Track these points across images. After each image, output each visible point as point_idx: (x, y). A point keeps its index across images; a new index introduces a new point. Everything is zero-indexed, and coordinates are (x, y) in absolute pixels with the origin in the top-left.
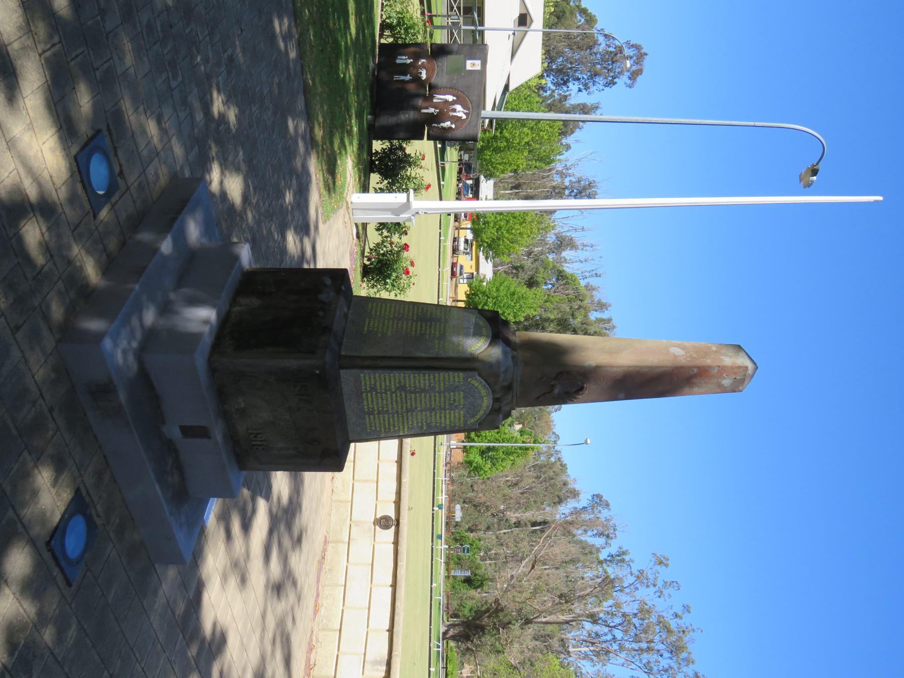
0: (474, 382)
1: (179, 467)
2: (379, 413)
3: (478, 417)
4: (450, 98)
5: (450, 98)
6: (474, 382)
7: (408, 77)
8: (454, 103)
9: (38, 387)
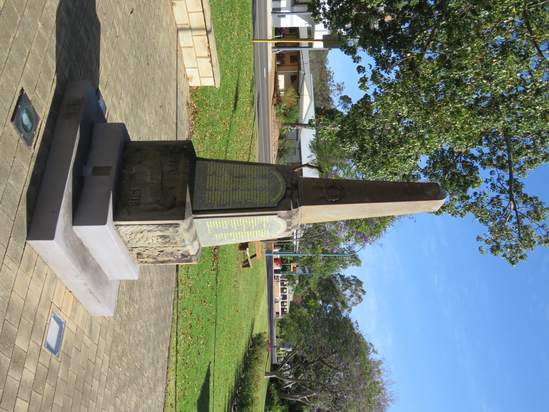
0: (274, 173)
2: (215, 190)
3: (277, 197)
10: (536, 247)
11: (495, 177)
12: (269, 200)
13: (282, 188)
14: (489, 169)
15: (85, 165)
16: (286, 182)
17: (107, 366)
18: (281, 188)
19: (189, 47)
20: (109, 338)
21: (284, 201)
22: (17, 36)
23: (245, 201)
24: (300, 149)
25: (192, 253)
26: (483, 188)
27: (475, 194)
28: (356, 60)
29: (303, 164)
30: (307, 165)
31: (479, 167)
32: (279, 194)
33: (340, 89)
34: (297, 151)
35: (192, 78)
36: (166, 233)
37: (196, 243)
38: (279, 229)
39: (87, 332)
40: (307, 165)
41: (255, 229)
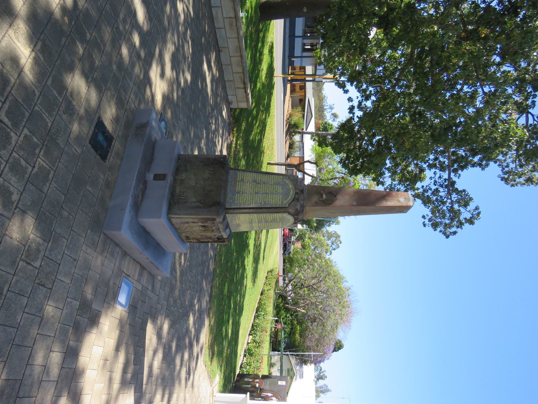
0: (286, 181)
1: (144, 191)
2: (243, 193)
3: (288, 200)
4: (270, 395)
5: (270, 395)
6: (286, 181)
7: (250, 386)
8: (271, 397)
9: (36, 44)
10: (465, 224)
11: (438, 176)
12: (282, 202)
13: (292, 193)
14: (433, 170)
15: (148, 172)
16: (295, 188)
17: (165, 309)
18: (291, 193)
19: (231, 81)
20: (167, 289)
21: (293, 203)
22: (95, 76)
23: (265, 202)
24: (303, 147)
25: (225, 236)
26: (426, 182)
27: (423, 187)
28: (346, 92)
29: (305, 160)
30: (308, 161)
31: (427, 168)
32: (290, 197)
33: (331, 108)
34: (302, 149)
35: (232, 102)
36: (206, 224)
37: (228, 230)
38: (289, 222)
39: (150, 288)
40: (308, 161)
41: (271, 221)
